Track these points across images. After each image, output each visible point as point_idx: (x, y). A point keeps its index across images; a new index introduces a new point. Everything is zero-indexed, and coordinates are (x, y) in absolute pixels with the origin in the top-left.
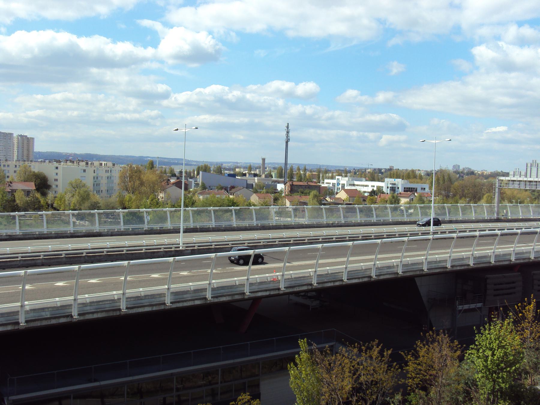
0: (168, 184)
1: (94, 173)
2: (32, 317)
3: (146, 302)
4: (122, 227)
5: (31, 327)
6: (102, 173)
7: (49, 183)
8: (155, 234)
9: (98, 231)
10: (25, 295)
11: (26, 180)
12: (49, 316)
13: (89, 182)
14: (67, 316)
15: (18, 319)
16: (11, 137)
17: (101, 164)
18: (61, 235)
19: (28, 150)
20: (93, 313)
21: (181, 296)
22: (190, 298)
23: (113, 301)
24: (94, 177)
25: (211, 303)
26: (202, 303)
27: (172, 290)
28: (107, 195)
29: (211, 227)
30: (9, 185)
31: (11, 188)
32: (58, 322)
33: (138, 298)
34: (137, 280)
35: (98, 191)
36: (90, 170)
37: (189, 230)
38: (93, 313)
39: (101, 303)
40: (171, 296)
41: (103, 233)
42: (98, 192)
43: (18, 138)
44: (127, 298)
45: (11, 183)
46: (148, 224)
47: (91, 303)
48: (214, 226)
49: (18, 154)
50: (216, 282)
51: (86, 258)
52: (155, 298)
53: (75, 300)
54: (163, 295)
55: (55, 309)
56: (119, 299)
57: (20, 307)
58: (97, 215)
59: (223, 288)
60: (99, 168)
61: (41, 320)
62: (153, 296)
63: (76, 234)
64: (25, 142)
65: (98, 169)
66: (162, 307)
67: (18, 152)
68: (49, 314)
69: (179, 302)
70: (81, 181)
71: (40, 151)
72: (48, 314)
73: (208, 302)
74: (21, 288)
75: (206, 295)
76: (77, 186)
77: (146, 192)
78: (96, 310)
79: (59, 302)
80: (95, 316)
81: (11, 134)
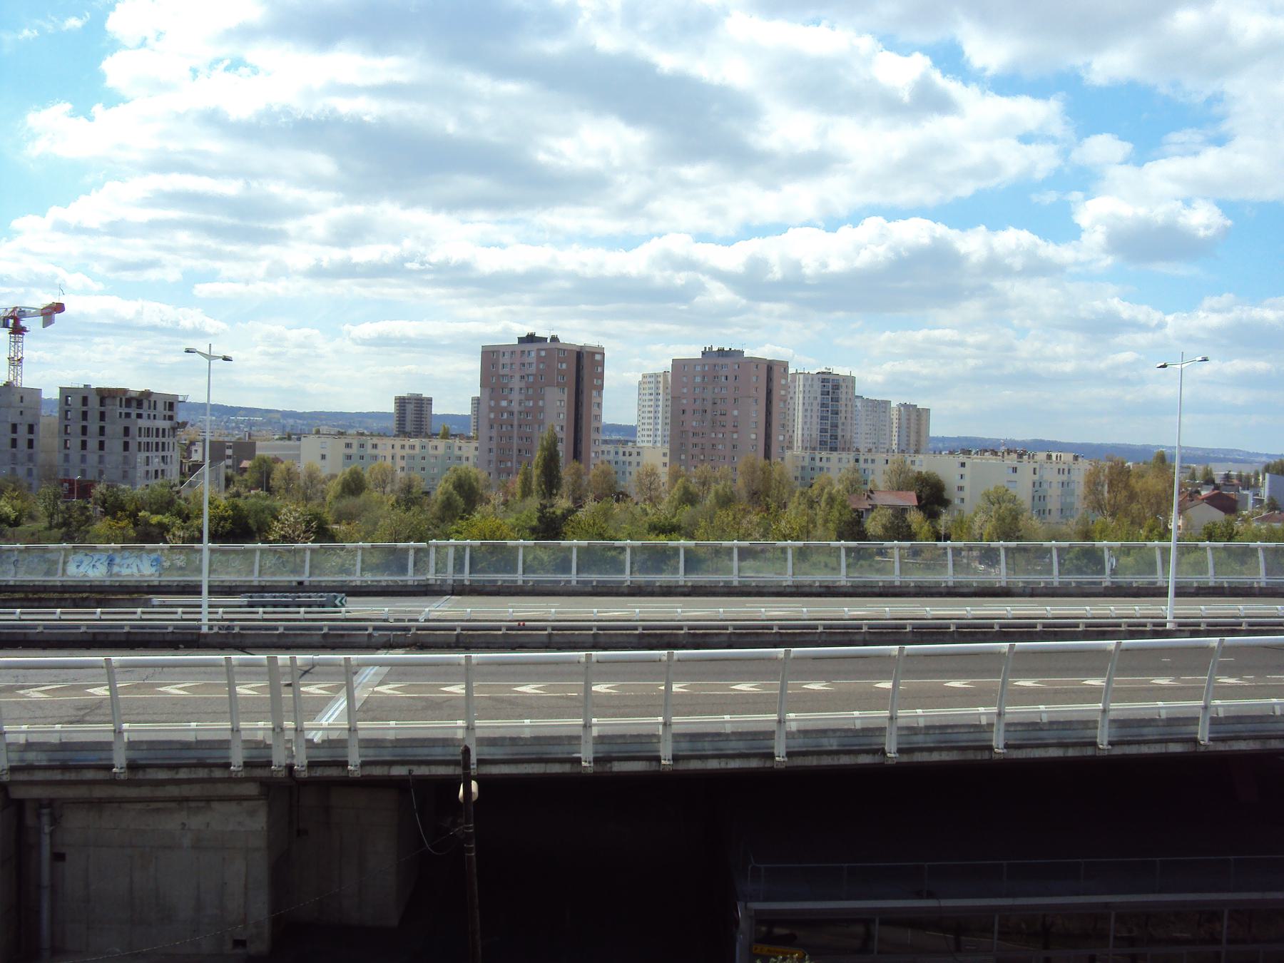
0: (1192, 500)
1: (1035, 473)
2: (800, 747)
3: (1050, 736)
4: (1056, 579)
5: (797, 767)
6: (1051, 476)
7: (946, 495)
8: (1125, 597)
9: (1004, 584)
10: (669, 704)
11: (901, 488)
12: (835, 748)
13: (1024, 493)
14: (874, 752)
15: (773, 748)
16: (886, 408)
17: (1049, 457)
18: (927, 590)
19: (918, 433)
20: (930, 750)
21: (1135, 731)
22: (1156, 737)
23: (977, 728)
24: (1034, 483)
25: (1209, 752)
26: (1186, 750)
27: (1112, 715)
28: (1061, 520)
29: (1255, 585)
30: (868, 496)
31: (872, 503)
32: (853, 763)
33: (1034, 726)
34: (1049, 689)
35: (1042, 512)
36: (1026, 467)
37: (1203, 591)
38: (930, 750)
39: (950, 731)
40: (1109, 728)
41: (1015, 590)
42: (1042, 513)
43: (900, 411)
44: (1008, 725)
45: (872, 492)
46: (1111, 574)
47: (928, 728)
48: (1263, 585)
49: (898, 441)
50: (1221, 705)
51: (956, 635)
52: (1074, 729)
53: (891, 718)
54: (1091, 725)
55: (850, 734)
56: (991, 725)
57: (1100, 714)
58: (1055, 553)
59: (1239, 719)
60: (1046, 465)
61: (820, 753)
62: (1067, 725)
63: (957, 590)
64: (913, 416)
65: (1041, 467)
66: (1089, 752)
67: (899, 436)
68: (835, 743)
69: (1129, 743)
70: (1007, 490)
71: (946, 436)
72: (833, 744)
73: (1202, 749)
74: (663, 688)
75: (1197, 733)
76: (996, 498)
77: (1142, 515)
78: (937, 745)
79: (795, 723)
80: (935, 757)
81: (888, 403)
